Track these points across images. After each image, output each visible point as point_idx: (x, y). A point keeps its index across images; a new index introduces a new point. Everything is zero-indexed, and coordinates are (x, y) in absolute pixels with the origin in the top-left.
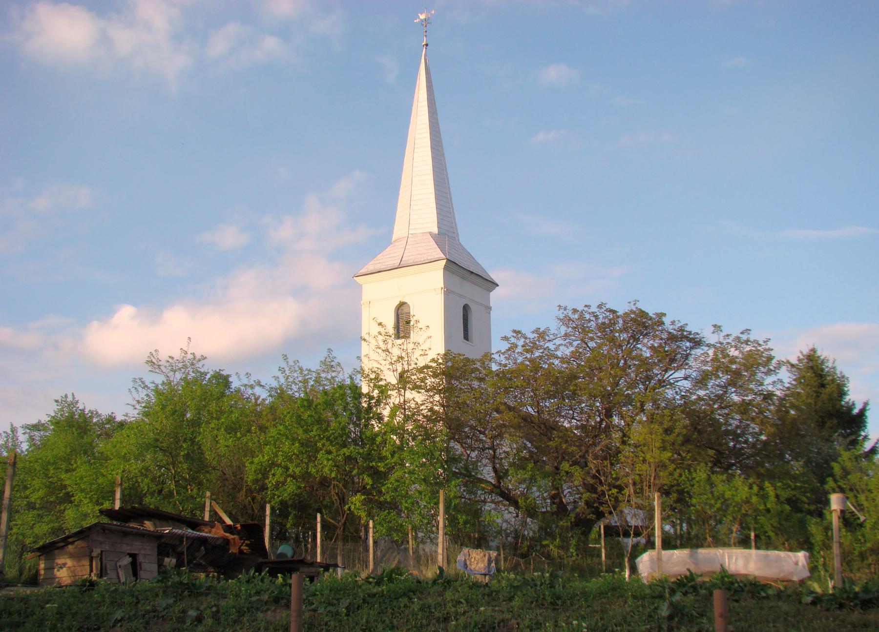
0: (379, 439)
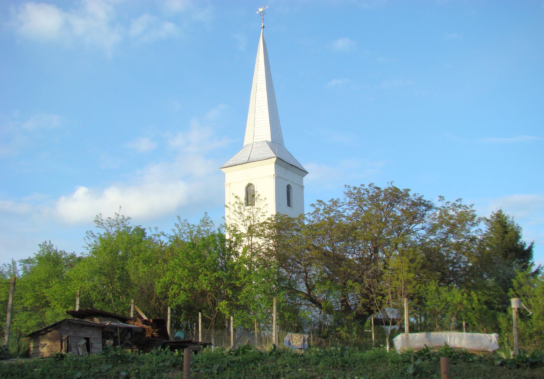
0: (236, 267)
